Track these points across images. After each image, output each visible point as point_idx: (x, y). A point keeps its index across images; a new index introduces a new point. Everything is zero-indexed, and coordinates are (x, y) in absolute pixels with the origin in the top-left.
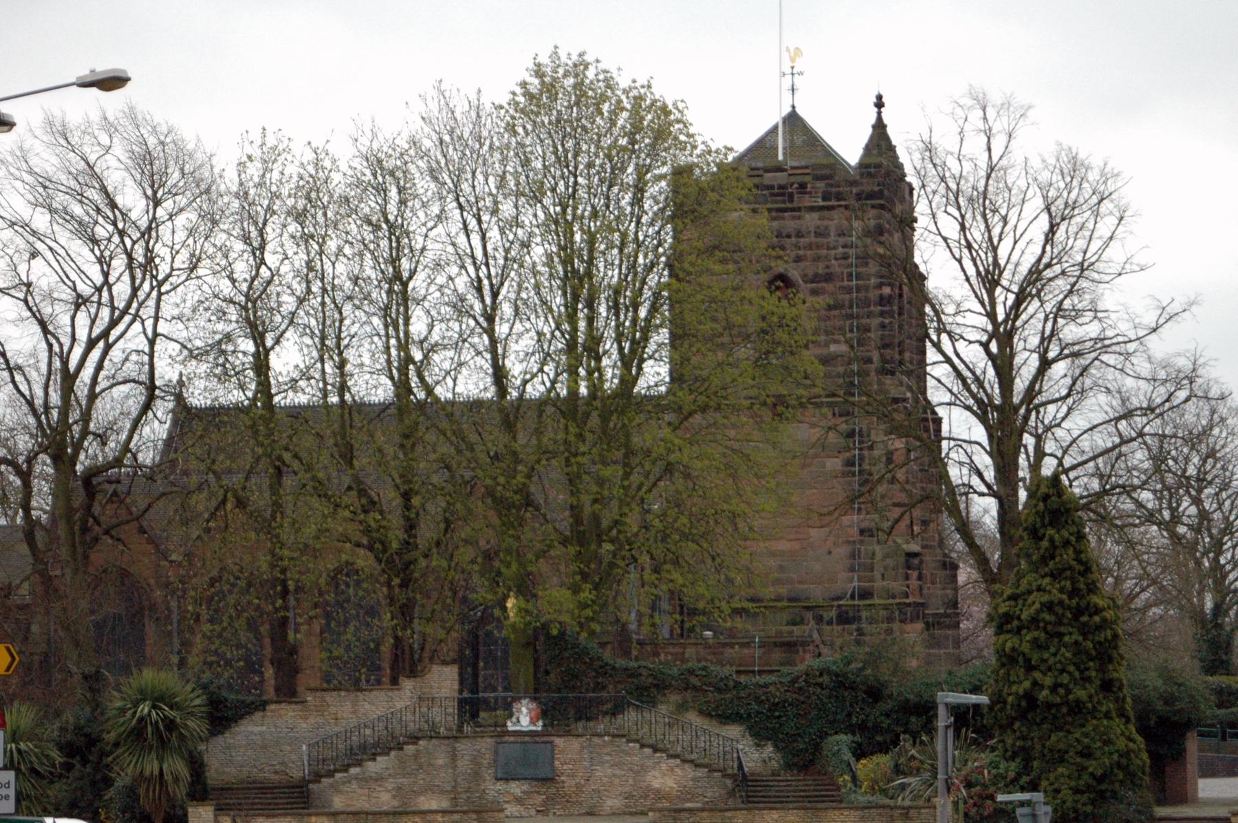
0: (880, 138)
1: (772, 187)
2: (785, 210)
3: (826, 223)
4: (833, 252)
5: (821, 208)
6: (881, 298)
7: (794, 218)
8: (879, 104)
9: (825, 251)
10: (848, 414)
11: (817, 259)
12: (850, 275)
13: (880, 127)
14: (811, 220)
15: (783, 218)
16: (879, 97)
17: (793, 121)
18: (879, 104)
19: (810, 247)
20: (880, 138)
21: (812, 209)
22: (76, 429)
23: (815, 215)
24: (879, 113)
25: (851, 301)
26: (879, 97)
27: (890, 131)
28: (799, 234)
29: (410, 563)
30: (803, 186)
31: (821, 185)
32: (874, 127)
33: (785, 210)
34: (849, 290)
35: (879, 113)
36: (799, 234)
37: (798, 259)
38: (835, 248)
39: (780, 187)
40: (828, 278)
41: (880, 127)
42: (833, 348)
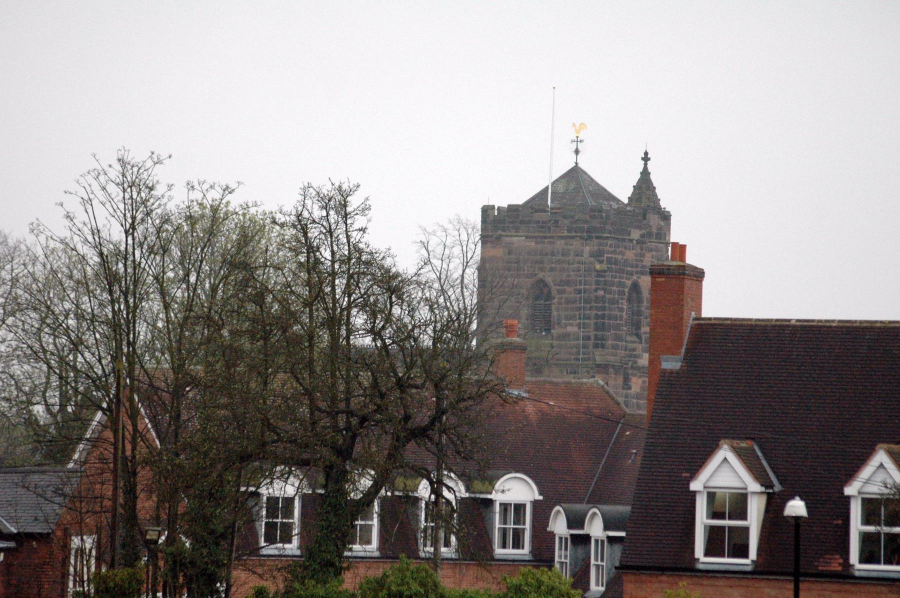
0: (645, 186)
1: (539, 222)
2: (545, 237)
3: (569, 247)
4: (572, 266)
5: (566, 237)
6: (597, 297)
7: (550, 242)
8: (646, 158)
9: (567, 266)
10: (575, 373)
11: (562, 270)
12: (580, 281)
13: (645, 173)
14: (560, 244)
15: (544, 243)
16: (646, 153)
17: (575, 174)
18: (646, 158)
19: (558, 262)
20: (645, 186)
21: (561, 238)
22: (151, 567)
23: (563, 242)
24: (646, 165)
25: (580, 299)
26: (646, 153)
27: (652, 177)
28: (553, 254)
29: (340, 187)
30: (556, 222)
31: (566, 222)
32: (641, 173)
33: (545, 237)
34: (580, 292)
35: (646, 165)
36: (553, 254)
37: (552, 270)
38: (573, 263)
39: (544, 222)
40: (568, 283)
41: (645, 173)
42: (569, 329)
